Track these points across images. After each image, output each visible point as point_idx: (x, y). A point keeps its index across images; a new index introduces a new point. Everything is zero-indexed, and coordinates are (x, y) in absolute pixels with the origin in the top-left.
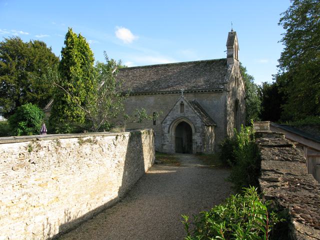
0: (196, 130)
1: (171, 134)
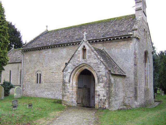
0: (98, 79)
1: (73, 83)
